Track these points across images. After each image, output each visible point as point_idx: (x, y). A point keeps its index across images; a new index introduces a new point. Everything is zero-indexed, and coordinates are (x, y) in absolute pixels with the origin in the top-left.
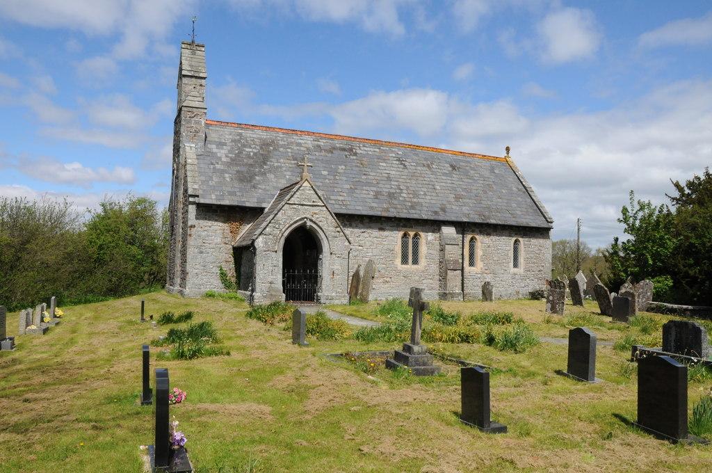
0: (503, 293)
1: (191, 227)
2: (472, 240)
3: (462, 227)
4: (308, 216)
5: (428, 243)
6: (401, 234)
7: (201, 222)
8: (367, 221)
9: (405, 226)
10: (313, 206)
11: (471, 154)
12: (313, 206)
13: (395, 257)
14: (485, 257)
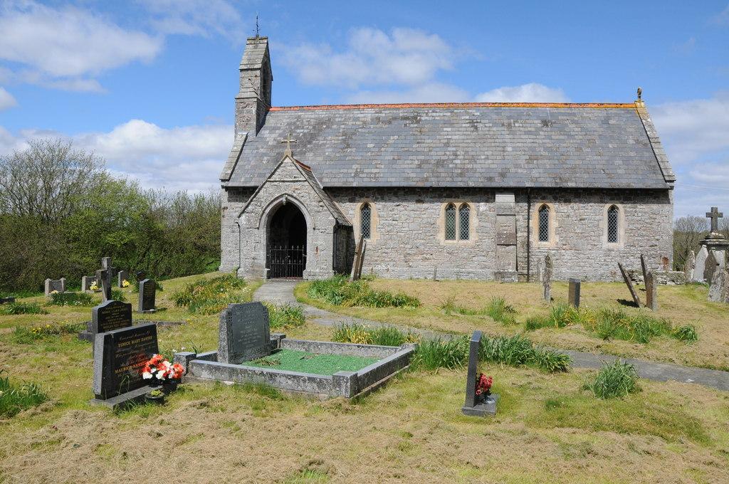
0: (590, 275)
1: (224, 208)
2: (544, 208)
3: (525, 194)
4: (290, 192)
5: (479, 214)
6: (444, 205)
7: (233, 203)
8: (374, 194)
9: (449, 196)
10: (294, 181)
11: (580, 104)
12: (294, 181)
13: (437, 232)
14: (562, 229)
